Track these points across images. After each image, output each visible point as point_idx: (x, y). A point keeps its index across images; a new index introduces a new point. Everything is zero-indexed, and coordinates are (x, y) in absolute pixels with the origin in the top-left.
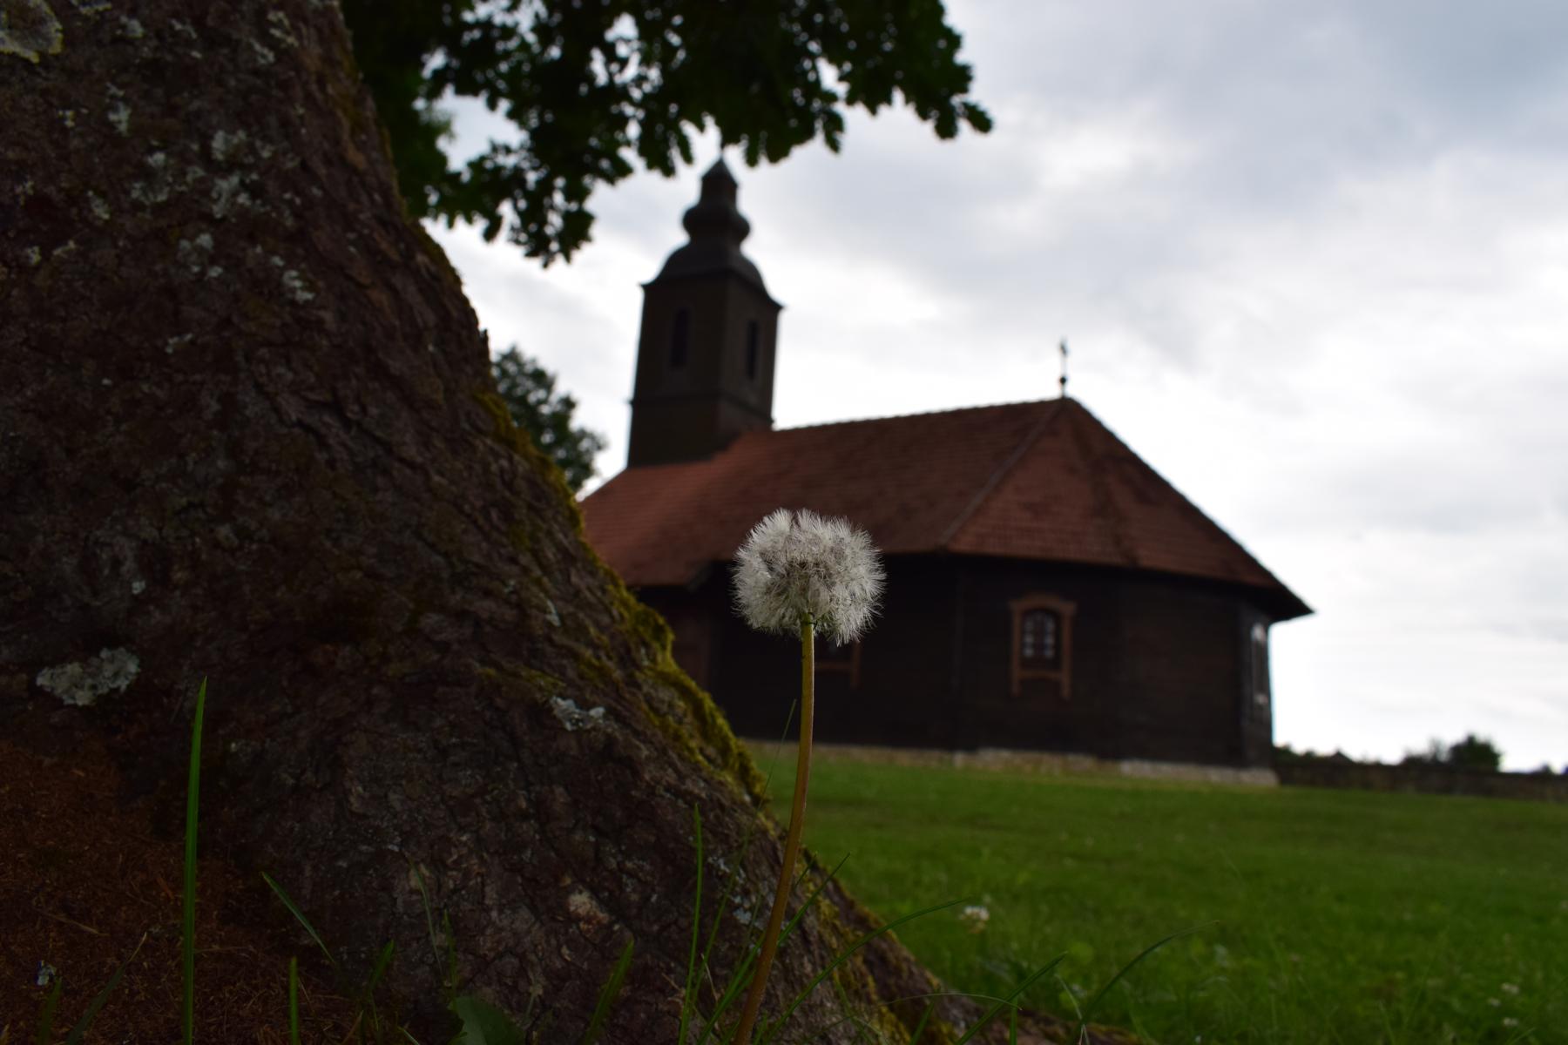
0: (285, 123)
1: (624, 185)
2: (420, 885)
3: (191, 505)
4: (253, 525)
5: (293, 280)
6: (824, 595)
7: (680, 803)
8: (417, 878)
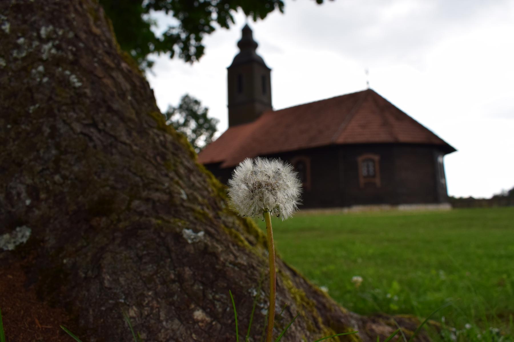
0: (68, 21)
1: (214, 34)
2: (134, 315)
3: (43, 170)
4: (67, 173)
5: (74, 79)
6: (272, 199)
7: (236, 269)
8: (133, 312)
